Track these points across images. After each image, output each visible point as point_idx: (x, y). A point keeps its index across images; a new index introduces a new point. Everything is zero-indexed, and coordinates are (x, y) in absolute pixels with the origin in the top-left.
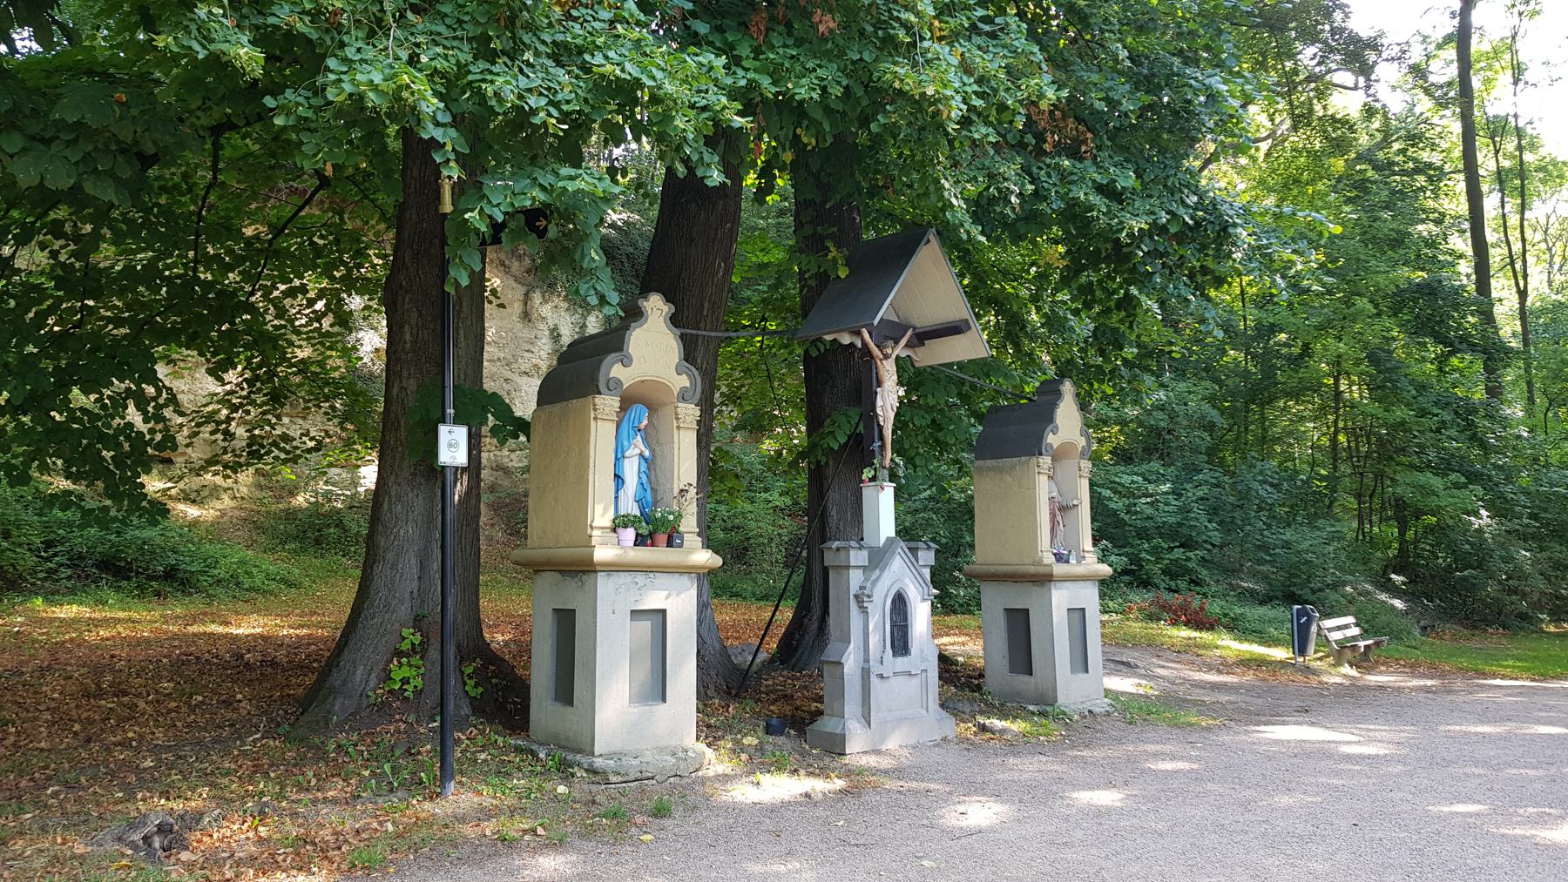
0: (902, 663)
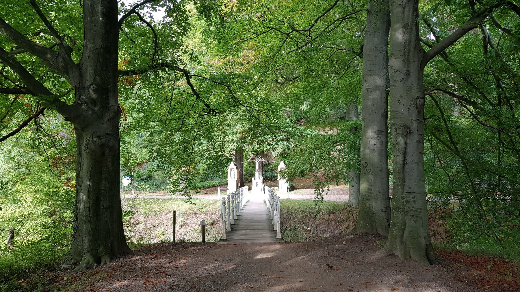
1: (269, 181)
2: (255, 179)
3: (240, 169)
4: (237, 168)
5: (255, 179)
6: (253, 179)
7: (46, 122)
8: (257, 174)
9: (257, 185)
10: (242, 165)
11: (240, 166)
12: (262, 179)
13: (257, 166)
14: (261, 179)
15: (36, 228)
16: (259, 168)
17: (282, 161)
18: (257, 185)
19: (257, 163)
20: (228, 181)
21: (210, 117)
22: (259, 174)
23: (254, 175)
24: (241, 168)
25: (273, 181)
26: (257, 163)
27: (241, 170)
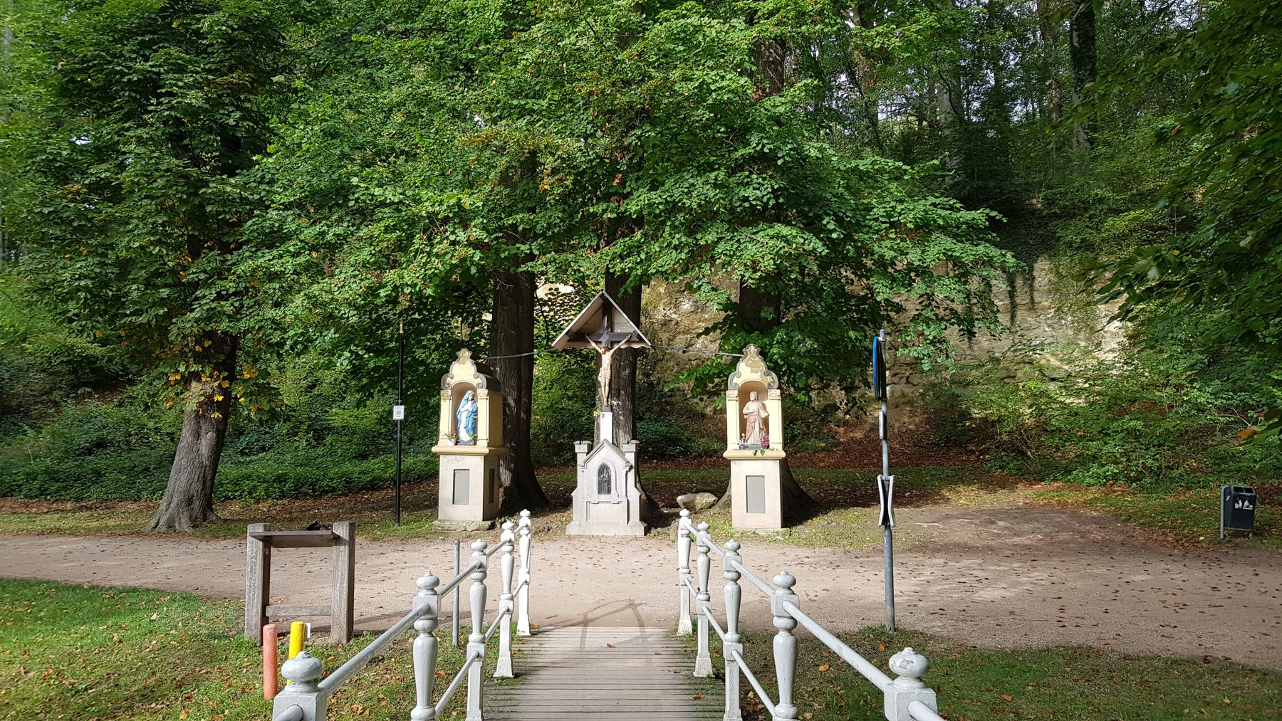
0: (604, 497)
1: (651, 458)
2: (590, 448)
3: (514, 394)
4: (492, 386)
5: (590, 448)
6: (581, 448)
7: (28, 445)
8: (605, 423)
9: (604, 485)
10: (525, 382)
11: (514, 384)
12: (630, 449)
13: (604, 375)
14: (625, 448)
15: (102, 171)
16: (614, 392)
17: (752, 349)
18: (604, 485)
19: (606, 359)
20: (437, 456)
21: (41, 284)
22: (616, 424)
23: (588, 433)
24: (519, 390)
25: (673, 458)
26: (606, 359)
27: (518, 401)
